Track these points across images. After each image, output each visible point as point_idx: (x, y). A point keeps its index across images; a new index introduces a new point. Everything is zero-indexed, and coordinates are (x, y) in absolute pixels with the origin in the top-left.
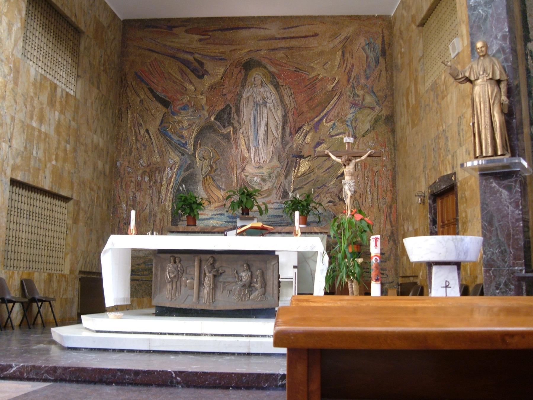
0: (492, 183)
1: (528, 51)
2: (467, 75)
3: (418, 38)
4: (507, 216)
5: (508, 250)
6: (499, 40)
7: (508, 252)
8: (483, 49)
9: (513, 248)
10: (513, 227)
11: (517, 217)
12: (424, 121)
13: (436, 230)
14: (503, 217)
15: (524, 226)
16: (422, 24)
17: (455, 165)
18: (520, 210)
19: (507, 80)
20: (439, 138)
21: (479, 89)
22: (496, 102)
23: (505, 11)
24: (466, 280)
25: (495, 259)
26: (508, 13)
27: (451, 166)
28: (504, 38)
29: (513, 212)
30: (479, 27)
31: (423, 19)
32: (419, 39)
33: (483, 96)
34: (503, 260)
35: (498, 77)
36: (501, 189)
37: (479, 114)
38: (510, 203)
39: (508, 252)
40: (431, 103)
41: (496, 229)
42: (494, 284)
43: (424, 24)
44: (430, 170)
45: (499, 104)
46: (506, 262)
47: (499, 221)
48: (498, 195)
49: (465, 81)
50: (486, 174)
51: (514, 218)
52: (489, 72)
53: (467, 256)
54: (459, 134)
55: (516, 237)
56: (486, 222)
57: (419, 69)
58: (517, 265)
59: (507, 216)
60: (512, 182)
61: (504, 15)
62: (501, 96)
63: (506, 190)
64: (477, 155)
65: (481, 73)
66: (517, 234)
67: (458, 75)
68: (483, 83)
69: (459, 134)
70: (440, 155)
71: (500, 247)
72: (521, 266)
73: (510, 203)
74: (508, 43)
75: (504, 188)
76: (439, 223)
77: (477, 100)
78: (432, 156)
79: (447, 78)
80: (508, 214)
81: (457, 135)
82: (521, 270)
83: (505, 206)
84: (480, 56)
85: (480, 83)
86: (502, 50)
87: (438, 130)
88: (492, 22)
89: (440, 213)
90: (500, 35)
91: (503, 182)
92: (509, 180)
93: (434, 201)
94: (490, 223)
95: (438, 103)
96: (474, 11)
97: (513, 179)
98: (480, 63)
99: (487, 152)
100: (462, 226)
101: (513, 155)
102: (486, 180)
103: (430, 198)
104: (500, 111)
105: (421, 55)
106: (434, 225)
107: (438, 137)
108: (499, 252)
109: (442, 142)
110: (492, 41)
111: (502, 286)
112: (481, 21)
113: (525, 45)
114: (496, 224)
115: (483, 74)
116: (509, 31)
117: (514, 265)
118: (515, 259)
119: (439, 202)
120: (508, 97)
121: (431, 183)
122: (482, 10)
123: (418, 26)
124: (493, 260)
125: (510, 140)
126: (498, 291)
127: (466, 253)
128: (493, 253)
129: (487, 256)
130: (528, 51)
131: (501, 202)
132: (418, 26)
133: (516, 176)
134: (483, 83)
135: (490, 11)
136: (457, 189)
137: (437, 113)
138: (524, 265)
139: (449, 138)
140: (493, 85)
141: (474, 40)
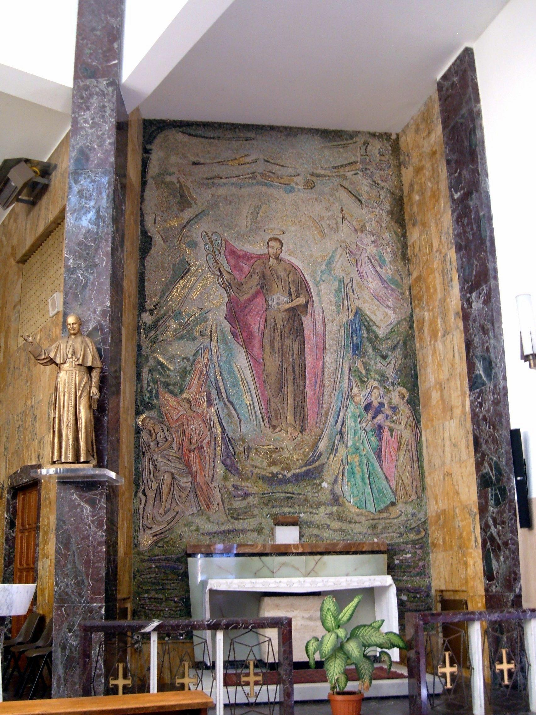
0: (72, 494)
1: (141, 323)
2: (52, 355)
3: (16, 277)
4: (86, 537)
5: (86, 581)
6: (98, 315)
7: (86, 584)
8: (75, 326)
9: (92, 579)
10: (94, 552)
11: (100, 540)
12: (11, 388)
13: (14, 535)
14: (82, 539)
15: (108, 552)
16: (24, 260)
17: (41, 454)
18: (103, 531)
19: (102, 368)
20: (26, 415)
21: (64, 377)
22: (85, 394)
23: (109, 280)
24: (43, 608)
25: (70, 592)
26: (112, 283)
27: (37, 456)
28: (104, 313)
29: (95, 533)
30: (76, 296)
31: (25, 255)
32: (18, 280)
33: (68, 386)
34: (79, 594)
35: (89, 364)
36: (82, 503)
37: (62, 407)
38: (93, 522)
39: (86, 584)
40: (21, 367)
41: (74, 553)
42: (66, 625)
43: (26, 261)
44: (13, 454)
45: (87, 397)
46: (83, 597)
47: (78, 544)
48: (78, 510)
49: (49, 363)
50: (65, 482)
51: (95, 541)
52: (79, 355)
53: (11, 610)
54: (49, 415)
55: (96, 565)
56: (62, 543)
57: (13, 318)
58: (96, 601)
59: (86, 537)
60: (97, 495)
61: (107, 286)
62: (90, 389)
63: (89, 505)
64: (55, 460)
65: (70, 356)
66: (99, 562)
67: (40, 355)
68: (71, 369)
69: (49, 415)
70: (25, 438)
71: (76, 577)
72: (101, 602)
73: (93, 522)
74: (108, 321)
75: (86, 502)
76: (18, 523)
77: (61, 389)
78: (17, 437)
79: (42, 341)
80: (89, 535)
81: (47, 416)
82: (100, 608)
83: (86, 524)
84: (71, 334)
85: (67, 368)
86: (99, 328)
87: (25, 404)
88: (92, 291)
89: (20, 514)
90: (99, 309)
91: (86, 494)
92: (93, 492)
93: (14, 497)
94: (67, 545)
95: (29, 369)
96: (72, 274)
97: (98, 492)
98: (70, 343)
99: (66, 457)
100: (44, 536)
101: (100, 465)
102: (65, 490)
103: (8, 492)
104: (87, 406)
105: (17, 300)
106: (11, 528)
107: (24, 414)
108: (74, 583)
109: (29, 420)
110: (90, 315)
111: (75, 628)
112: (80, 288)
113: (140, 315)
114: (74, 547)
115: (72, 357)
116: (111, 307)
117: (92, 600)
118: (93, 593)
119: (20, 497)
120: (100, 389)
121: (12, 472)
122: (82, 274)
123: (18, 262)
124: (67, 594)
125: (98, 441)
126: (70, 634)
127: (9, 606)
128: (67, 585)
129: (60, 588)
130: (141, 323)
131: (82, 519)
132: (18, 262)
133: (102, 488)
134: (71, 369)
135: (91, 277)
136: (41, 486)
137: (27, 381)
138: (104, 601)
139: (37, 418)
140: (83, 373)
141: (68, 310)
